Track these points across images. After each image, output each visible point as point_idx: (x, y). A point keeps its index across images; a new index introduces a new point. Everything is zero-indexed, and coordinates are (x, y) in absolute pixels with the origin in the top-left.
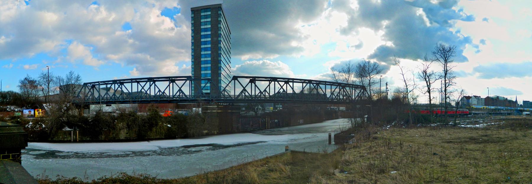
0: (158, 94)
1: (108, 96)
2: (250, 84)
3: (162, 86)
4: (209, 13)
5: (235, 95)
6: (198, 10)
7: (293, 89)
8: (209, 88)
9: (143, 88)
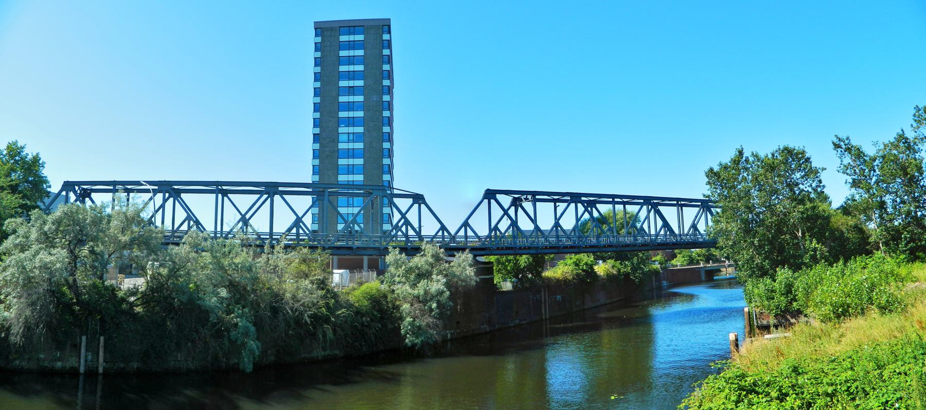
0: (185, 227)
1: (470, 233)
2: (486, 201)
3: (203, 206)
4: (360, 37)
5: (271, 233)
6: (332, 29)
7: (534, 221)
8: (343, 138)
9: (245, 221)
